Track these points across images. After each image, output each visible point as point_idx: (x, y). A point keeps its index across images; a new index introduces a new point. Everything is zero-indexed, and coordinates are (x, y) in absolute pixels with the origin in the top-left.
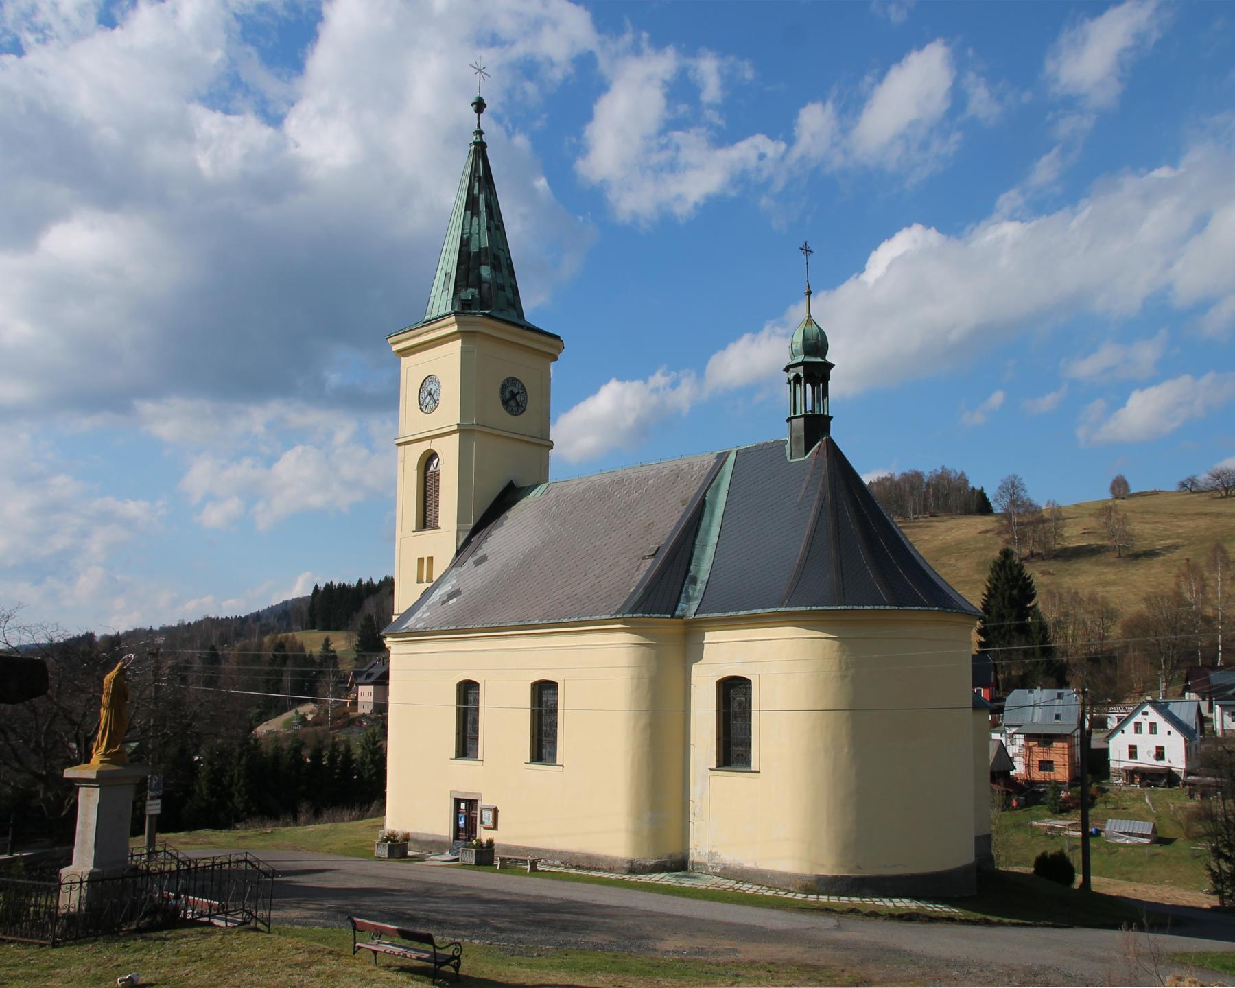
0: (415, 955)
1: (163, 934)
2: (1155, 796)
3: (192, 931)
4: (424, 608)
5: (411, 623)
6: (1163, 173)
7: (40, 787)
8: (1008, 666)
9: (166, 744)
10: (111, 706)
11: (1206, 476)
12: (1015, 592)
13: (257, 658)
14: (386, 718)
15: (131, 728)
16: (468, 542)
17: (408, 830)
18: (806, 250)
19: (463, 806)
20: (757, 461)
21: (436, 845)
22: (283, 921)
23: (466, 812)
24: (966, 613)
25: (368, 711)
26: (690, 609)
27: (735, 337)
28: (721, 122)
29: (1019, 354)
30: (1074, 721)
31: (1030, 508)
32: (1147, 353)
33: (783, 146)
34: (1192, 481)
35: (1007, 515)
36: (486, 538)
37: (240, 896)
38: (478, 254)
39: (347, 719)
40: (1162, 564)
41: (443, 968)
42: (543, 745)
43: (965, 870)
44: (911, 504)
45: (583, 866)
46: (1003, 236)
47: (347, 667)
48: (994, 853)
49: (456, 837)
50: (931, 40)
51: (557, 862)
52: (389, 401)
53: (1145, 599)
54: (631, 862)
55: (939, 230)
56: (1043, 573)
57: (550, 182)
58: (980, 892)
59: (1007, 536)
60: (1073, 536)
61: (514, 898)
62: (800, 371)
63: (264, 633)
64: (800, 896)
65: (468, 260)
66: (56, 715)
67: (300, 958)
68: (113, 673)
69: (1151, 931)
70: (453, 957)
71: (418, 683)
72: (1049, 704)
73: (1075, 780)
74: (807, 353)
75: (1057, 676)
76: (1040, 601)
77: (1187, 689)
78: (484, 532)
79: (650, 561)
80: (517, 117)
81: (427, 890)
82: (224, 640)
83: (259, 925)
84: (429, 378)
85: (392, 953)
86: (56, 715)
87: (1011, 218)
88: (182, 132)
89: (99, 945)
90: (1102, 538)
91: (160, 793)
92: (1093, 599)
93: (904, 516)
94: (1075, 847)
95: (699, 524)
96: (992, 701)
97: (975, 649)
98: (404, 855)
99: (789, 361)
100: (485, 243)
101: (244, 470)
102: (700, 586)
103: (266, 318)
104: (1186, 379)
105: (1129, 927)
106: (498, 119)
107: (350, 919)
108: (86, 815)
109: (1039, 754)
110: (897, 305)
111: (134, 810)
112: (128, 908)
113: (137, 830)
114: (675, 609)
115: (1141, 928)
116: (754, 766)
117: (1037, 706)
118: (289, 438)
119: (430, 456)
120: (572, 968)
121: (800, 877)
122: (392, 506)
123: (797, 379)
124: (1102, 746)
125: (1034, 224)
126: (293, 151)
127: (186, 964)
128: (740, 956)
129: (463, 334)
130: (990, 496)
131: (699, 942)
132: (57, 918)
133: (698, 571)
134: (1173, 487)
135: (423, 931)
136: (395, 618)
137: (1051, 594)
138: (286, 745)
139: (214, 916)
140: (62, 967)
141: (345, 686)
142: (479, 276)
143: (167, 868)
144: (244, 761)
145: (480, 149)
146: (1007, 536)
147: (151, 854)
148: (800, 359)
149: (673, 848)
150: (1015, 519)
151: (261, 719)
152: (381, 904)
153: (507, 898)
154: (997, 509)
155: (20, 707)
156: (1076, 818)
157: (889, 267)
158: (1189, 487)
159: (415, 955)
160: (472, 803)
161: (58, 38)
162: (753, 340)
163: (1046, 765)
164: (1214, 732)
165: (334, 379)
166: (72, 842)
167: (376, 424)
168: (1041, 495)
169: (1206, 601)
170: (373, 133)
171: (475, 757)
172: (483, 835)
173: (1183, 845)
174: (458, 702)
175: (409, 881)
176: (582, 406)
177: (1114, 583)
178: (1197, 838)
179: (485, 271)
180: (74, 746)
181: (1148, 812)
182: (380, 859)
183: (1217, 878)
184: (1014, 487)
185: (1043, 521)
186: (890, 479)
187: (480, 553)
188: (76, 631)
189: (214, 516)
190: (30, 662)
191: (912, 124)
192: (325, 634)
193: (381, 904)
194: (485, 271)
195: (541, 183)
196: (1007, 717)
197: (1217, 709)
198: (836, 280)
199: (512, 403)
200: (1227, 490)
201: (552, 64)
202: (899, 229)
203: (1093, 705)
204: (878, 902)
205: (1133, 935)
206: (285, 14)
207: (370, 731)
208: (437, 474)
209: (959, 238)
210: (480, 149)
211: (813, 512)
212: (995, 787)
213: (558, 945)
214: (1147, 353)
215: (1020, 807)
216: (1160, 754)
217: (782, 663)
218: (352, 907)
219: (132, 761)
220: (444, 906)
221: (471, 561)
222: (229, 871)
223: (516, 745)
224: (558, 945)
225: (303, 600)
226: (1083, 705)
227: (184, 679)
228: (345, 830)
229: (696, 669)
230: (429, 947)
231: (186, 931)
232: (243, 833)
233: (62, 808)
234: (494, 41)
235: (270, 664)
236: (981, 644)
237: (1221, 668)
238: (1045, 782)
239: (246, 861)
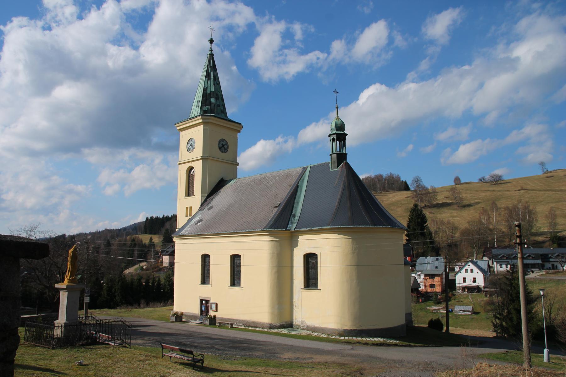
0: (186, 358)
1: (91, 347)
2: (473, 296)
3: (102, 346)
4: (188, 226)
5: (183, 232)
6: (466, 67)
7: (47, 290)
8: (417, 248)
9: (91, 276)
10: (71, 261)
11: (488, 176)
12: (419, 220)
13: (125, 245)
14: (174, 268)
15: (79, 270)
16: (205, 201)
17: (183, 311)
18: (336, 92)
19: (204, 302)
20: (318, 171)
21: (194, 317)
22: (135, 344)
23: (205, 304)
24: (401, 228)
25: (167, 265)
26: (293, 227)
27: (309, 124)
28: (302, 46)
29: (418, 131)
30: (443, 269)
31: (424, 188)
32: (465, 131)
33: (326, 55)
34: (484, 178)
35: (415, 191)
36: (212, 199)
37: (119, 334)
38: (210, 94)
39: (159, 268)
40: (474, 209)
41: (197, 364)
42: (235, 279)
43: (402, 326)
44: (379, 186)
45: (251, 326)
46: (410, 88)
47: (159, 249)
48: (413, 320)
49: (201, 314)
50: (380, 19)
51: (241, 324)
52: (176, 148)
53: (468, 223)
54: (270, 324)
55: (386, 85)
56: (430, 213)
57: (237, 68)
58: (409, 334)
59: (416, 199)
60: (441, 199)
61: (224, 338)
62: (335, 136)
63: (127, 235)
64: (337, 337)
65: (206, 96)
66: (52, 264)
67: (142, 358)
68: (72, 249)
69: (471, 347)
70: (201, 360)
71: (186, 255)
72: (433, 263)
73: (443, 291)
74: (337, 130)
75: (436, 252)
76: (429, 223)
77: (484, 256)
78: (212, 197)
79: (277, 209)
80: (225, 45)
81: (190, 334)
82: (113, 237)
83: (127, 345)
84: (191, 139)
85: (177, 358)
86: (52, 264)
87: (413, 82)
88: (103, 53)
89: (69, 350)
90: (452, 200)
91: (89, 294)
92: (449, 223)
93: (376, 191)
94: (444, 316)
95: (296, 194)
96: (412, 262)
97: (404, 242)
98: (181, 321)
99: (330, 133)
100: (213, 90)
101: (121, 174)
102: (297, 218)
103: (131, 118)
104: (480, 141)
105: (463, 346)
106: (218, 46)
107: (161, 344)
108: (63, 301)
109: (430, 282)
110: (370, 112)
111: (80, 300)
112: (79, 337)
113: (81, 308)
114: (287, 227)
115: (468, 346)
116: (319, 287)
117: (429, 263)
118: (137, 162)
119: (191, 169)
120: (247, 364)
121: (337, 330)
122: (176, 187)
123: (333, 140)
124: (453, 278)
125: (421, 84)
126: (142, 58)
127: (100, 358)
128: (314, 360)
129: (204, 123)
130: (409, 183)
131: (298, 355)
132: (54, 339)
133: (296, 212)
134: (477, 181)
135: (189, 349)
136: (177, 230)
137: (433, 221)
138: (135, 278)
139: (110, 341)
140: (56, 356)
141: (158, 256)
142: (210, 101)
143: (92, 323)
144: (120, 283)
145: (211, 56)
146: (416, 199)
147: (86, 317)
148: (334, 132)
149: (286, 319)
150: (419, 193)
151: (127, 267)
152: (173, 339)
153: (222, 338)
154: (412, 188)
155: (40, 261)
156: (443, 305)
157: (368, 99)
158: (482, 180)
159: (186, 358)
160: (207, 301)
161: (63, 24)
162: (316, 125)
163: (432, 286)
164: (494, 272)
165: (155, 140)
166: (58, 311)
167: (170, 157)
168: (428, 183)
169: (490, 223)
170: (173, 51)
171: (208, 284)
172: (212, 313)
173: (483, 315)
174: (202, 262)
175: (184, 330)
176: (250, 149)
177: (456, 217)
178: (488, 311)
179: (213, 100)
180: (58, 276)
181: (470, 302)
182: (172, 322)
183: (495, 326)
184: (418, 180)
185: (429, 193)
186: (370, 177)
187: (210, 205)
188: (59, 233)
189: (109, 191)
190: (43, 244)
191: (374, 48)
192: (150, 236)
193: (173, 339)
194: (213, 100)
195: (234, 68)
196: (418, 268)
197: (495, 263)
198: (347, 103)
199: (223, 148)
200: (496, 181)
201: (239, 27)
202: (371, 85)
203: (450, 263)
204: (368, 339)
205: (464, 348)
206: (142, 12)
207: (168, 273)
208: (193, 175)
209: (394, 88)
210: (211, 56)
211: (340, 190)
212: (413, 294)
213: (242, 356)
214: (465, 131)
215: (423, 302)
216: (475, 280)
217: (330, 248)
218: (162, 340)
219: (79, 282)
220: (197, 340)
221: (206, 208)
222: (115, 325)
223: (225, 280)
224: (242, 356)
225: (142, 222)
226: (446, 263)
227: (98, 252)
228: (159, 311)
229: (296, 250)
230: (192, 356)
231: (100, 346)
232: (120, 311)
233: (54, 298)
234: (217, 19)
235: (130, 247)
236: (407, 240)
237: (496, 248)
238: (432, 292)
239: (121, 321)
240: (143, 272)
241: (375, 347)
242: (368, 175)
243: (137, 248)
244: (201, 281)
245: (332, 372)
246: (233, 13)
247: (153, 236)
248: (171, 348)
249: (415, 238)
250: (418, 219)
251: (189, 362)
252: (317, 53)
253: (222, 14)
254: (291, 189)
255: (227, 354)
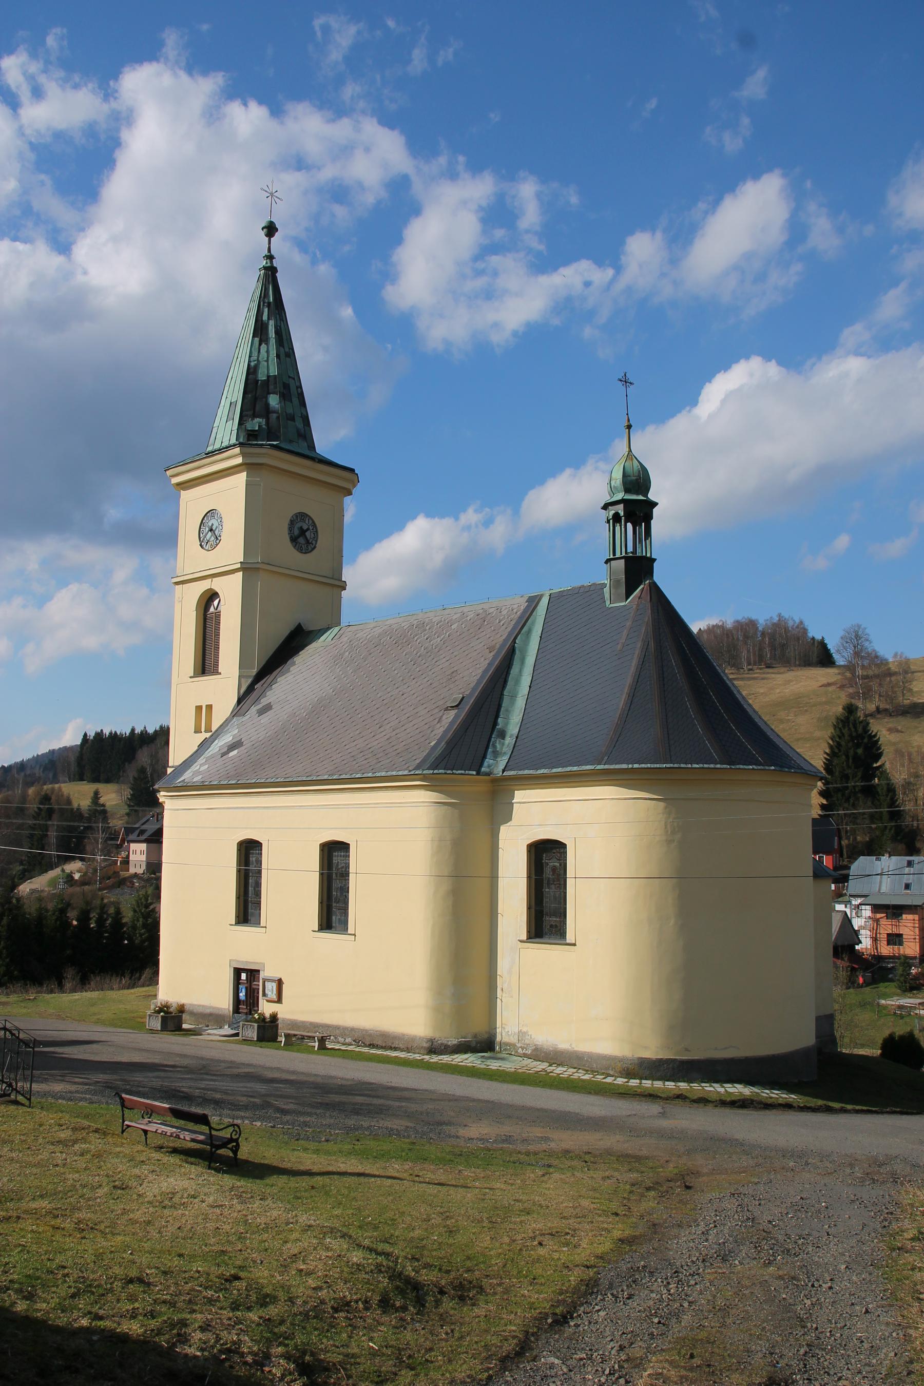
0: (189, 1136)
4: (202, 760)
8: (853, 831)
12: (860, 751)
13: (21, 811)
14: (159, 879)
16: (250, 689)
17: (183, 1000)
18: (625, 381)
20: (572, 605)
22: (45, 1094)
23: (247, 980)
24: (809, 774)
25: (140, 871)
26: (497, 765)
27: (553, 472)
28: (542, 247)
31: (875, 660)
35: (850, 667)
36: (270, 685)
39: (118, 879)
41: (222, 1151)
42: (333, 911)
44: (744, 654)
45: (377, 1044)
46: (846, 370)
47: (117, 823)
48: (837, 1034)
49: (236, 1010)
50: (769, 170)
51: (348, 1040)
52: (168, 539)
54: (431, 1041)
55: (779, 363)
56: (890, 730)
59: (851, 690)
62: (620, 509)
63: (28, 784)
64: (620, 1081)
65: (255, 390)
70: (231, 1140)
71: (194, 841)
74: (627, 491)
76: (887, 761)
79: (453, 713)
81: (204, 1067)
83: (20, 1098)
84: (211, 513)
85: (164, 1134)
87: (857, 353)
93: (737, 666)
96: (836, 869)
97: (816, 812)
99: (607, 499)
100: (274, 371)
102: (509, 741)
109: (887, 926)
114: (481, 765)
116: (570, 937)
118: (63, 576)
119: (210, 597)
120: (364, 1154)
121: (621, 1060)
123: (616, 518)
126: (80, 278)
128: (553, 1145)
129: (248, 466)
131: (507, 1129)
133: (507, 724)
136: (169, 770)
137: (899, 753)
138: (50, 906)
141: (116, 843)
142: (267, 405)
145: (270, 274)
146: (851, 690)
148: (620, 496)
149: (476, 1028)
150: (859, 672)
151: (25, 875)
154: (840, 660)
157: (723, 402)
159: (189, 1136)
160: (253, 974)
163: (895, 939)
165: (114, 513)
168: (888, 646)
171: (257, 923)
172: (266, 1008)
174: (239, 863)
175: (185, 1056)
179: (274, 401)
182: (152, 1031)
184: (857, 637)
185: (890, 674)
187: (264, 702)
191: (748, 256)
192: (93, 787)
194: (274, 401)
196: (853, 886)
198: (663, 414)
199: (301, 540)
201: (360, 185)
207: (142, 892)
208: (218, 615)
210: (270, 274)
212: (839, 962)
215: (867, 984)
217: (603, 827)
218: (120, 1083)
221: (254, 709)
224: (349, 1130)
225: (76, 745)
228: (116, 999)
229: (505, 832)
230: (205, 1129)
235: (35, 818)
236: (823, 807)
238: (893, 957)
240: (71, 890)
241: (727, 1111)
242: (714, 621)
243: (55, 822)
244: (237, 917)
245: (604, 1178)
246: (344, 151)
247: (101, 787)
248: (147, 1106)
249: (847, 800)
250: (855, 747)
251: (198, 1146)
252: (585, 265)
253: (313, 148)
254: (495, 657)
255: (306, 1124)
